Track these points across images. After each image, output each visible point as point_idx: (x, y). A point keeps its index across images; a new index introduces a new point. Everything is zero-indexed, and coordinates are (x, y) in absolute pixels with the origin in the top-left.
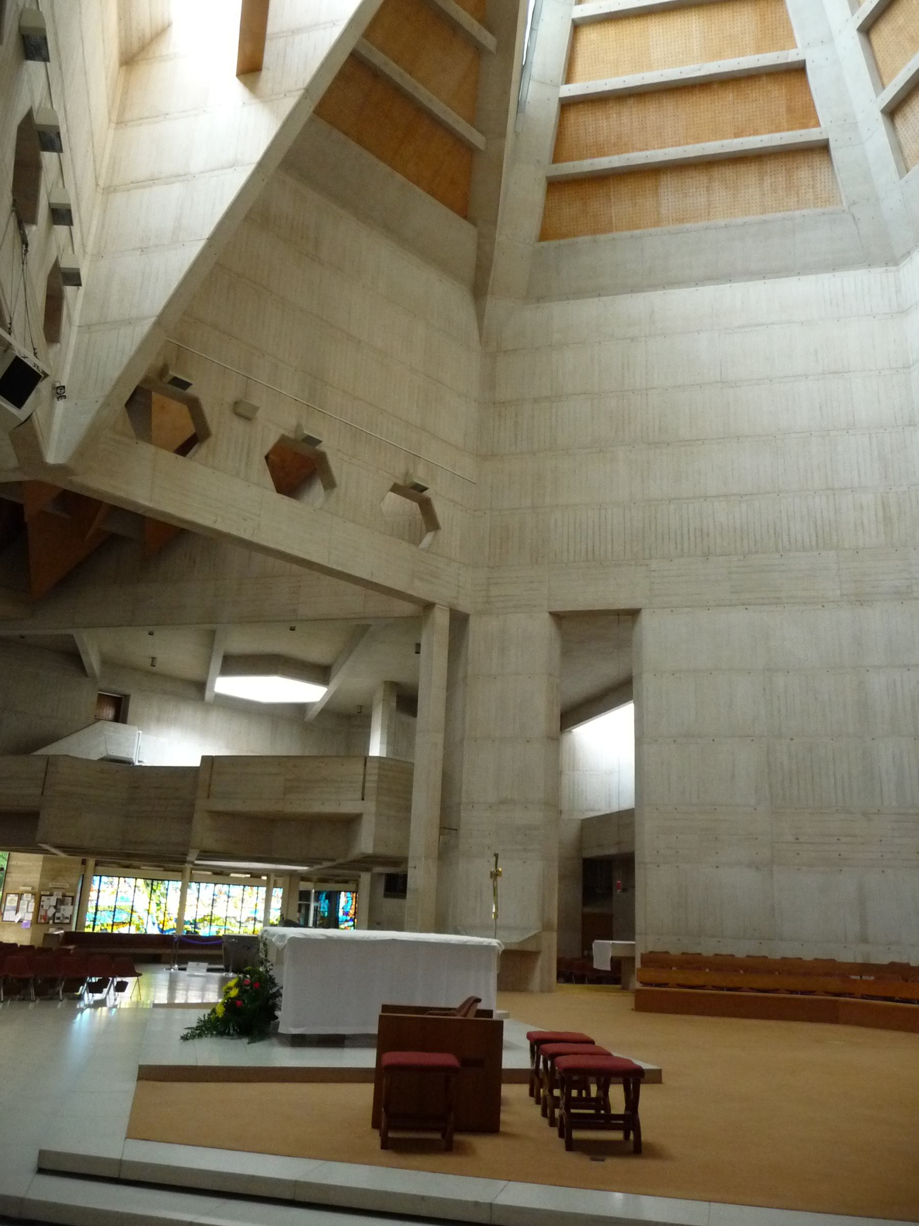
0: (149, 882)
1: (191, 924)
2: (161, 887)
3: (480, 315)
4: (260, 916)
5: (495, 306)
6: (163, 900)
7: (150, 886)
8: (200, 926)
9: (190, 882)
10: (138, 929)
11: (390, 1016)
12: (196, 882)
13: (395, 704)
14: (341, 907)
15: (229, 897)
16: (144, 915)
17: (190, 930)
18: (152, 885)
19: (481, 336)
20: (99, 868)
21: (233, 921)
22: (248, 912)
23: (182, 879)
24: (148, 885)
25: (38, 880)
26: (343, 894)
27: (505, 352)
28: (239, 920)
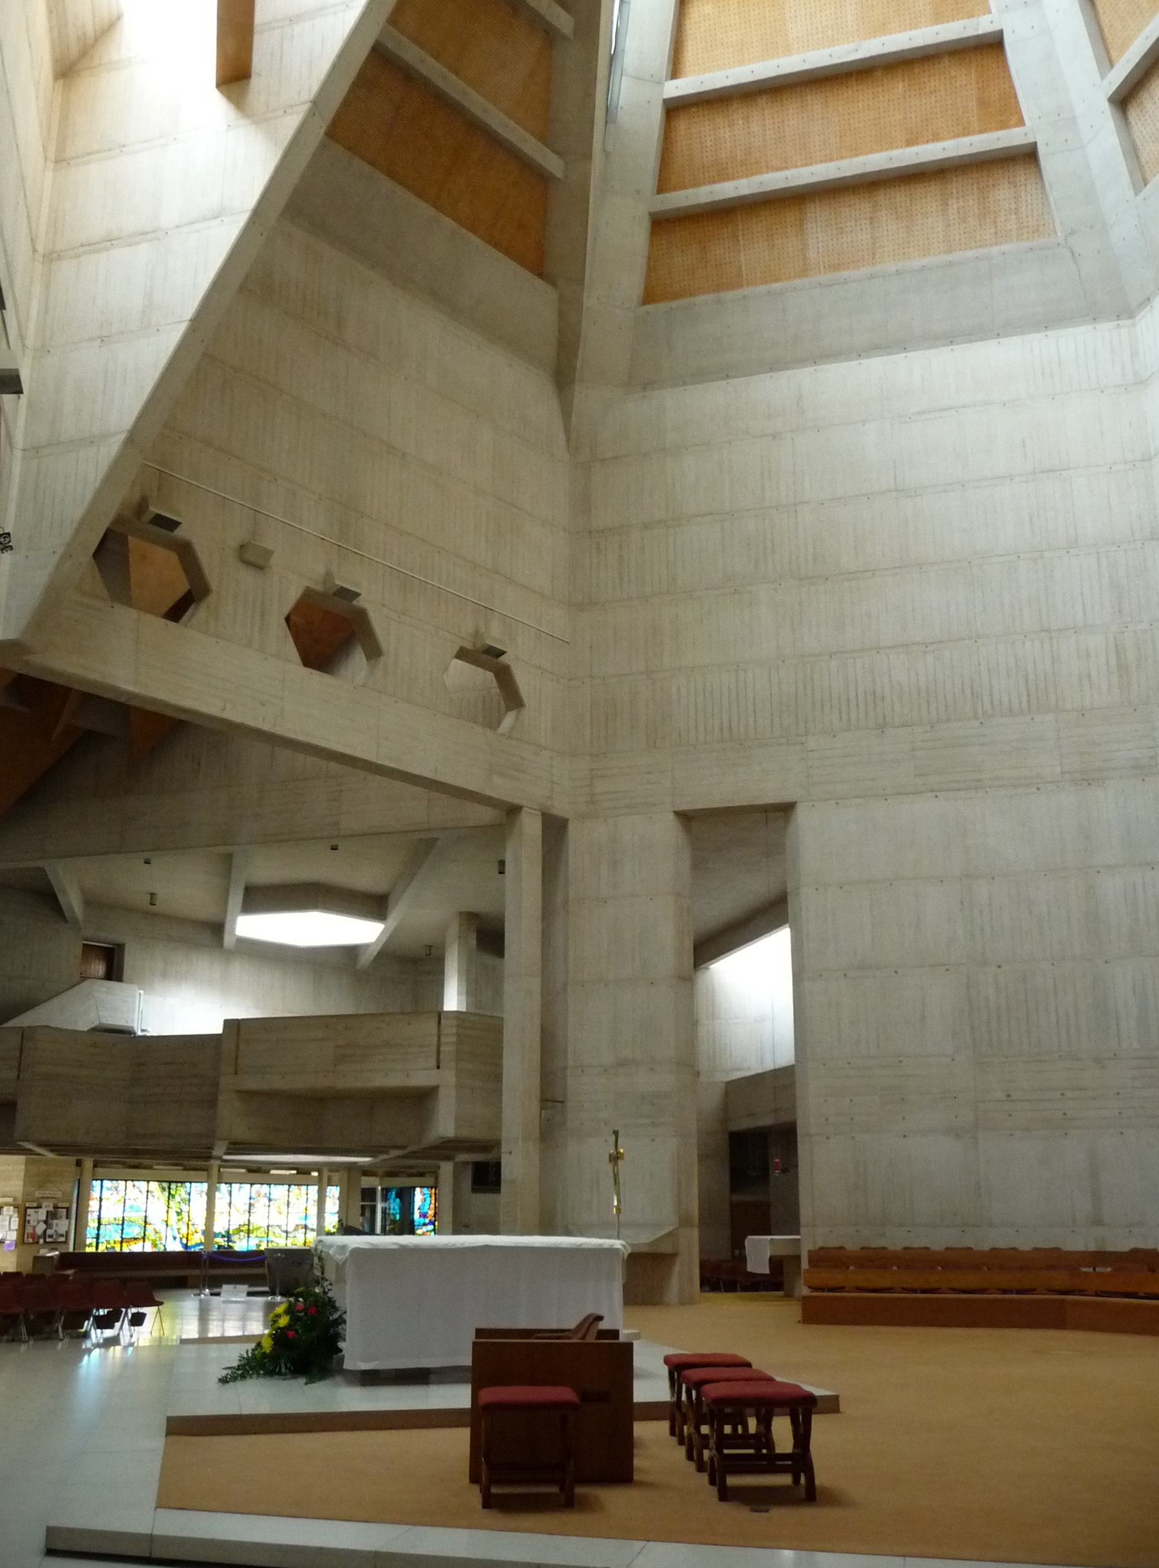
0: (165, 1185)
1: (223, 1236)
2: (181, 1192)
3: (566, 412)
4: (312, 1222)
5: (586, 397)
6: (185, 1208)
7: (167, 1190)
8: (234, 1238)
9: (218, 1183)
10: (155, 1245)
11: (487, 1342)
12: (226, 1183)
13: (474, 942)
14: (416, 1207)
15: (270, 1200)
16: (161, 1227)
17: (223, 1244)
18: (169, 1188)
19: (568, 440)
20: (99, 1170)
21: (277, 1230)
22: (295, 1219)
23: (208, 1180)
24: (164, 1189)
25: (21, 1189)
26: (418, 1190)
27: (602, 461)
28: (284, 1228)
